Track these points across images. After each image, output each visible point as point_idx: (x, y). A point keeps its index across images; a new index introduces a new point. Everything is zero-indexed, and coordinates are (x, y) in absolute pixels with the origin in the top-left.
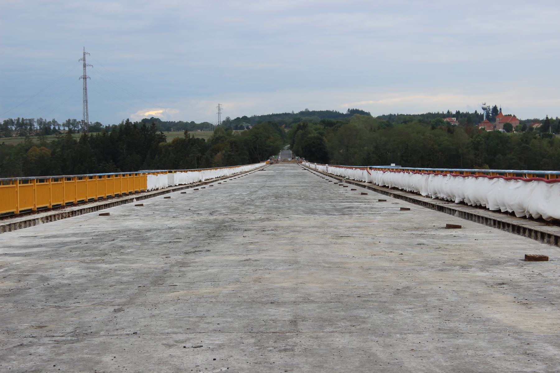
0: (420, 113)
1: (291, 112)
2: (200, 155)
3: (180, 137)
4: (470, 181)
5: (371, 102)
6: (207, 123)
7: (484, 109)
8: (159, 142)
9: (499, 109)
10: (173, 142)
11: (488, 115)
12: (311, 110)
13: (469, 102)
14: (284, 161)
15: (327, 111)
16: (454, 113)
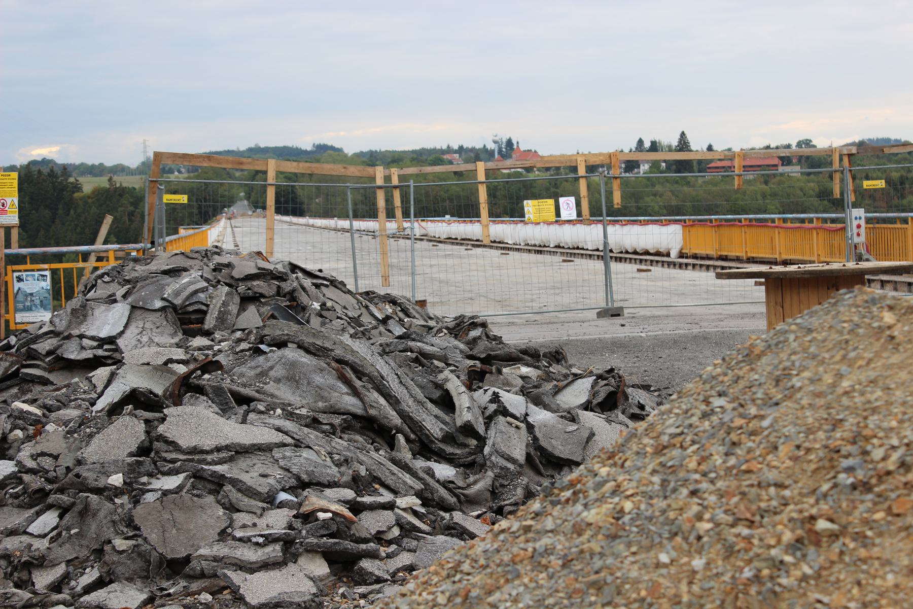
0: (411, 149)
1: (235, 149)
2: (132, 208)
3: (102, 185)
4: (636, 229)
5: (342, 133)
6: (121, 165)
7: (495, 142)
8: (74, 192)
9: (515, 142)
10: (94, 192)
11: (500, 151)
12: (262, 146)
13: (477, 133)
14: (243, 215)
15: (285, 147)
16: (456, 147)
